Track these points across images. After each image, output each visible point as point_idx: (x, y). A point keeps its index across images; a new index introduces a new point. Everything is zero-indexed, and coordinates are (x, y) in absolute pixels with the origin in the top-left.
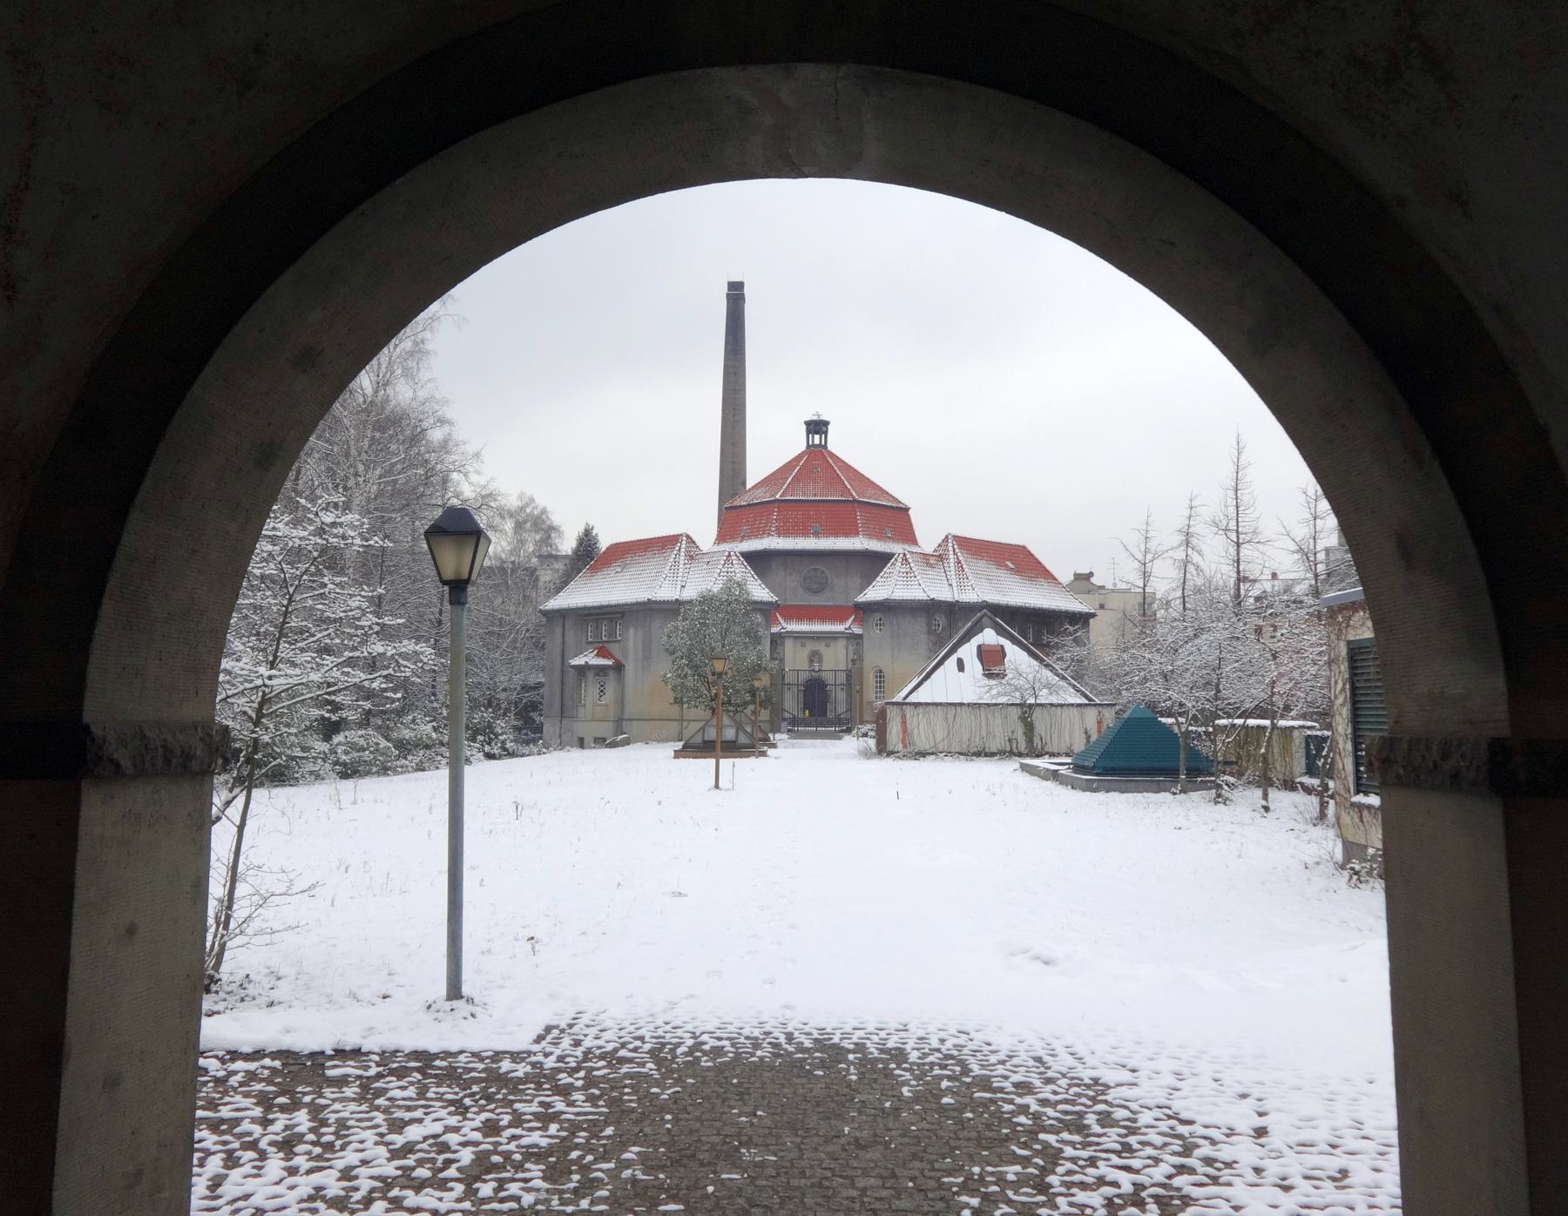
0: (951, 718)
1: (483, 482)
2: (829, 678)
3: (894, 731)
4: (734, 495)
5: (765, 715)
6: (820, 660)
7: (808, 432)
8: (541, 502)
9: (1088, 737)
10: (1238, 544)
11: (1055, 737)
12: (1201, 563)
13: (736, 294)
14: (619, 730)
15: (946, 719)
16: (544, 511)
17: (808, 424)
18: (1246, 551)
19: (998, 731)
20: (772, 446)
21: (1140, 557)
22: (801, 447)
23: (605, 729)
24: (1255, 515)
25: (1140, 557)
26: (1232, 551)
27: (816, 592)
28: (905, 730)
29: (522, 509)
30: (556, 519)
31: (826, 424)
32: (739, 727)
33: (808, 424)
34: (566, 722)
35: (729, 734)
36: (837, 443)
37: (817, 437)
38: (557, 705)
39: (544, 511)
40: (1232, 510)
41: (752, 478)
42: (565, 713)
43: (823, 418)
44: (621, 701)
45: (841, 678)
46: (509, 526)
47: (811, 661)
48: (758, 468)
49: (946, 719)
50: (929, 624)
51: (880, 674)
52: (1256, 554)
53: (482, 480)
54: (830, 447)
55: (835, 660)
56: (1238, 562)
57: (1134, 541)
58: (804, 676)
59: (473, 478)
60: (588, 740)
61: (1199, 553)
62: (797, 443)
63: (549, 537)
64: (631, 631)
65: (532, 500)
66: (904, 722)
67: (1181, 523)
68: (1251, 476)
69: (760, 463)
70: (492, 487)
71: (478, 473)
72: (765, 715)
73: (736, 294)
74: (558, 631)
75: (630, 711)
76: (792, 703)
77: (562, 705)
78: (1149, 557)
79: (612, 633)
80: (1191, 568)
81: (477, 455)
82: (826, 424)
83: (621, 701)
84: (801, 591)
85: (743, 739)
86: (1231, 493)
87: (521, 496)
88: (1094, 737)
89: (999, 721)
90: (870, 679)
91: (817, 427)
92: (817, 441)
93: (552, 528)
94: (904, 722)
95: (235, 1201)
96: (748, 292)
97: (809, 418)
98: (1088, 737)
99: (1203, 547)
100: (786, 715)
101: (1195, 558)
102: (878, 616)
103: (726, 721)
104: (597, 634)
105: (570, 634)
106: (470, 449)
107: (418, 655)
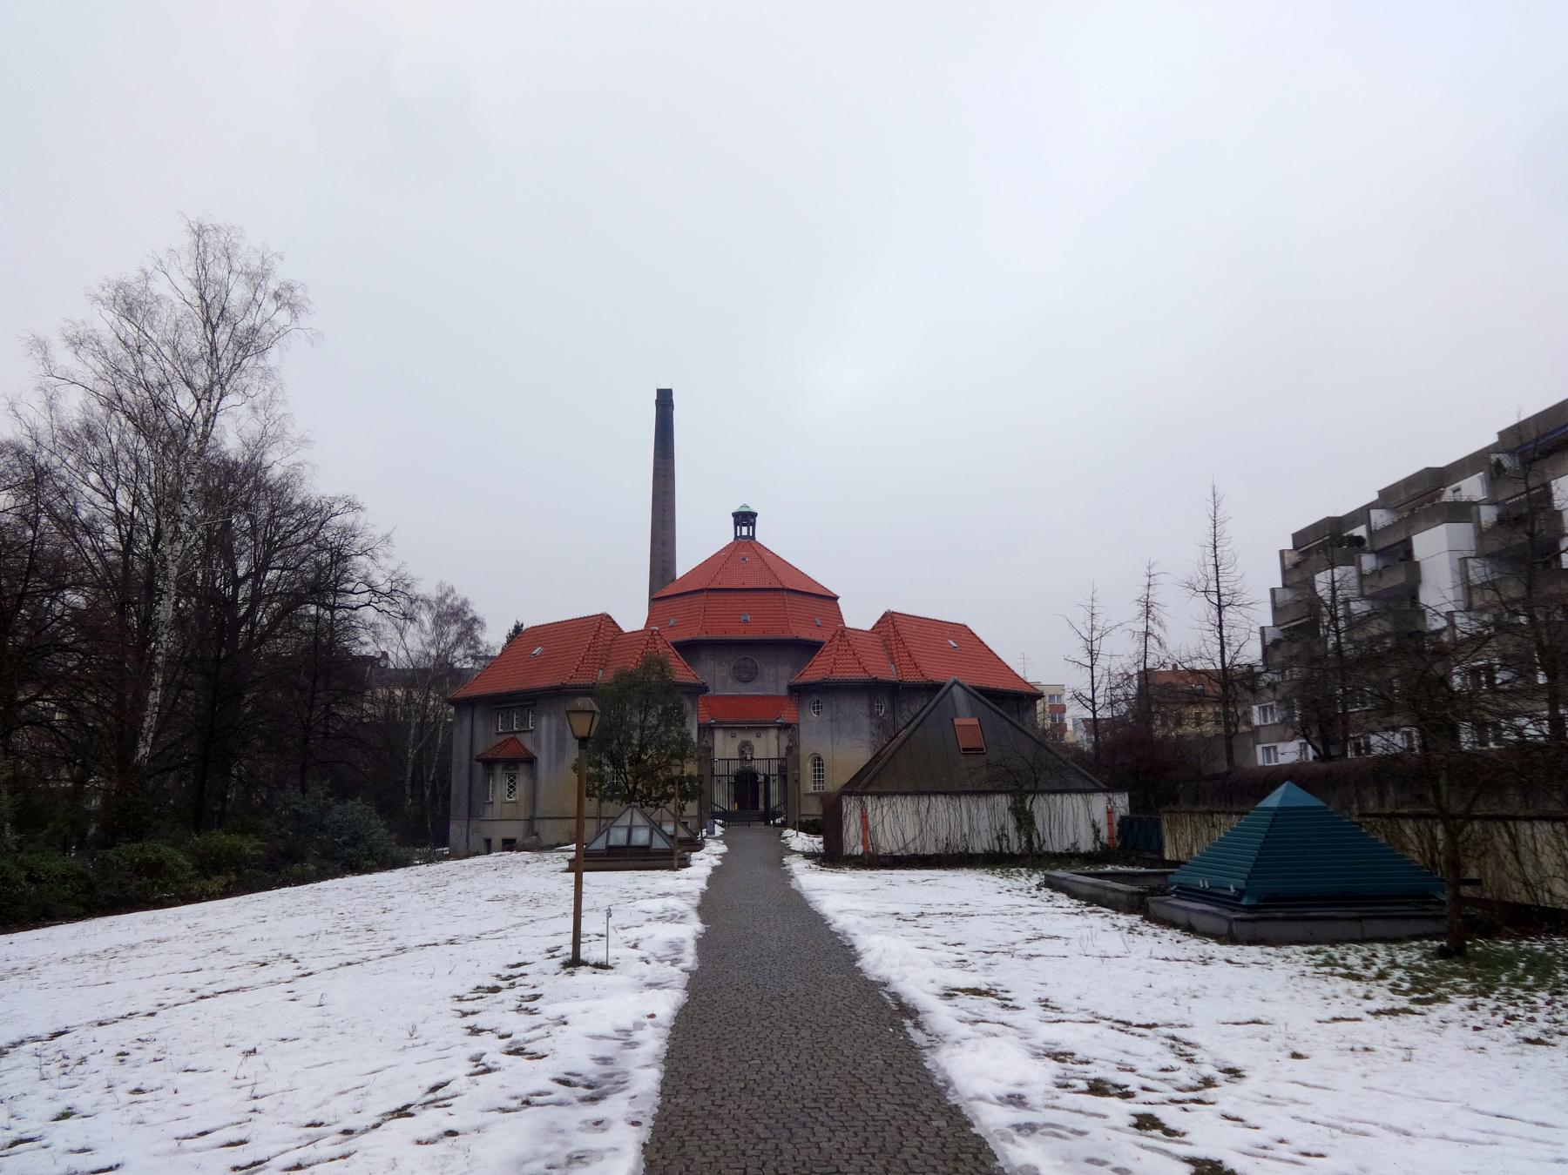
0: (923, 810)
2: (760, 768)
3: (852, 829)
4: (665, 584)
5: (691, 808)
6: (751, 749)
7: (736, 524)
8: (462, 592)
9: (1097, 832)
10: (1220, 608)
11: (1055, 832)
12: (1162, 635)
13: (665, 401)
14: (531, 830)
15: (918, 812)
16: (465, 603)
17: (735, 515)
18: (1228, 614)
19: (984, 824)
20: (701, 539)
21: (1087, 635)
22: (731, 539)
23: (515, 830)
24: (1238, 573)
25: (1087, 635)
26: (1214, 613)
27: (747, 681)
28: (865, 827)
29: (441, 600)
30: (477, 609)
31: (754, 515)
32: (656, 827)
33: (735, 515)
35: (641, 837)
36: (764, 534)
37: (745, 529)
39: (465, 603)
40: (1211, 570)
41: (680, 572)
42: (472, 813)
43: (753, 509)
44: (533, 799)
46: (426, 618)
47: (742, 752)
48: (687, 560)
49: (918, 812)
50: (871, 706)
51: (818, 761)
52: (1240, 618)
53: (392, 565)
54: (760, 538)
55: (767, 747)
56: (1220, 626)
58: (735, 767)
59: (382, 561)
61: (1160, 624)
62: (725, 535)
63: (471, 628)
65: (453, 590)
66: (864, 817)
67: (1141, 592)
68: (1228, 530)
69: (687, 560)
70: (402, 572)
71: (387, 556)
73: (665, 401)
74: (467, 721)
75: (542, 808)
76: (721, 797)
77: (470, 804)
78: (1096, 635)
80: (1152, 641)
81: (387, 539)
82: (754, 515)
83: (533, 799)
84: (730, 681)
85: (659, 843)
86: (1210, 550)
87: (440, 586)
88: (1104, 834)
89: (984, 812)
90: (808, 767)
91: (745, 518)
92: (745, 533)
93: (474, 620)
94: (864, 817)
95: (666, 895)
97: (736, 509)
98: (1097, 832)
99: (1163, 617)
100: (717, 809)
101: (1156, 629)
102: (815, 697)
103: (638, 820)
106: (378, 533)
107: (671, 806)
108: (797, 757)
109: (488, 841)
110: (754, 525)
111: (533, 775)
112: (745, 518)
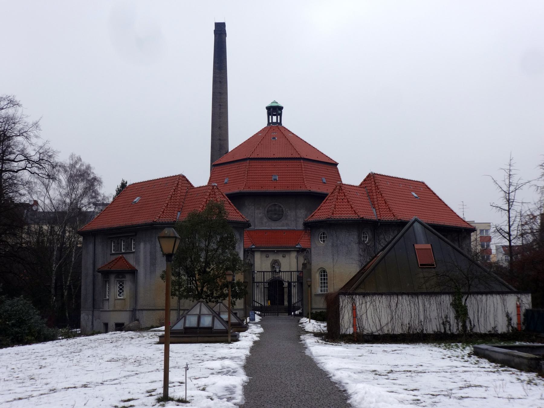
0: (393, 305)
1: (40, 144)
2: (285, 277)
4: (221, 155)
5: (239, 304)
6: (279, 265)
7: (269, 114)
8: (86, 160)
9: (510, 320)
11: (482, 320)
13: (220, 30)
14: (134, 318)
15: (390, 306)
16: (88, 167)
17: (268, 108)
20: (245, 125)
21: (505, 189)
22: (265, 124)
23: (124, 318)
25: (505, 189)
27: (275, 220)
28: (355, 316)
29: (73, 166)
30: (97, 171)
31: (281, 108)
32: (216, 315)
33: (268, 108)
34: (96, 313)
35: (207, 321)
36: (288, 121)
37: (275, 118)
38: (90, 300)
39: (88, 167)
41: (233, 144)
43: (280, 104)
45: (294, 278)
46: (63, 178)
47: (273, 267)
48: (235, 139)
49: (390, 306)
50: (359, 237)
51: (323, 273)
53: (40, 143)
54: (284, 124)
55: (289, 264)
57: (502, 178)
58: (268, 277)
59: (34, 140)
60: (112, 324)
62: (261, 122)
64: (142, 245)
65: (80, 159)
66: (354, 309)
70: (46, 147)
71: (37, 137)
72: (239, 304)
73: (220, 30)
74: (91, 246)
75: (142, 302)
76: (259, 297)
77: (94, 300)
78: (512, 188)
79: (128, 247)
82: (281, 108)
84: (265, 220)
85: (218, 326)
87: (72, 157)
88: (515, 321)
89: (434, 307)
90: (317, 277)
91: (275, 110)
93: (95, 179)
94: (354, 309)
96: (228, 29)
97: (269, 104)
98: (510, 320)
100: (257, 305)
102: (322, 231)
103: (205, 310)
104: (118, 248)
105: (99, 249)
106: (30, 121)
108: (310, 270)
109: (106, 325)
110: (280, 115)
111: (135, 281)
112: (275, 110)
